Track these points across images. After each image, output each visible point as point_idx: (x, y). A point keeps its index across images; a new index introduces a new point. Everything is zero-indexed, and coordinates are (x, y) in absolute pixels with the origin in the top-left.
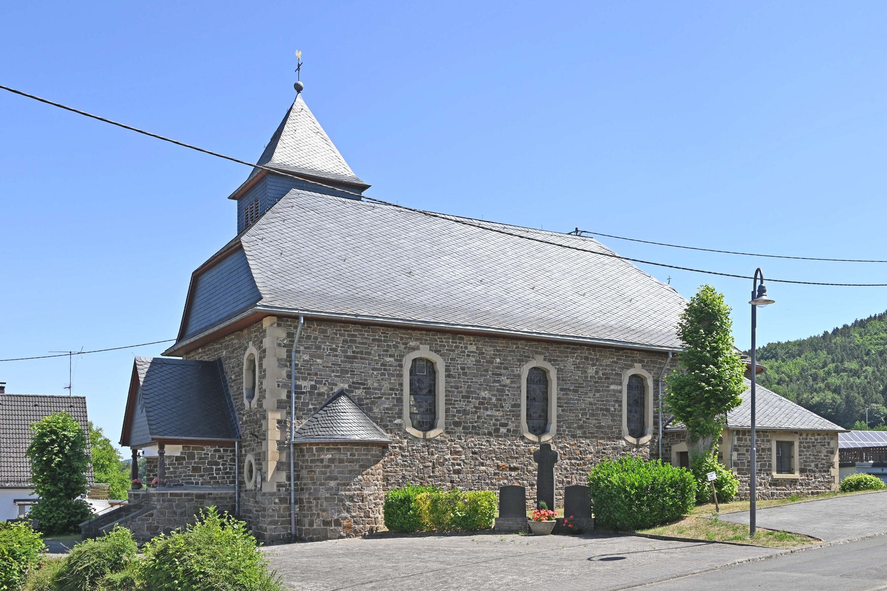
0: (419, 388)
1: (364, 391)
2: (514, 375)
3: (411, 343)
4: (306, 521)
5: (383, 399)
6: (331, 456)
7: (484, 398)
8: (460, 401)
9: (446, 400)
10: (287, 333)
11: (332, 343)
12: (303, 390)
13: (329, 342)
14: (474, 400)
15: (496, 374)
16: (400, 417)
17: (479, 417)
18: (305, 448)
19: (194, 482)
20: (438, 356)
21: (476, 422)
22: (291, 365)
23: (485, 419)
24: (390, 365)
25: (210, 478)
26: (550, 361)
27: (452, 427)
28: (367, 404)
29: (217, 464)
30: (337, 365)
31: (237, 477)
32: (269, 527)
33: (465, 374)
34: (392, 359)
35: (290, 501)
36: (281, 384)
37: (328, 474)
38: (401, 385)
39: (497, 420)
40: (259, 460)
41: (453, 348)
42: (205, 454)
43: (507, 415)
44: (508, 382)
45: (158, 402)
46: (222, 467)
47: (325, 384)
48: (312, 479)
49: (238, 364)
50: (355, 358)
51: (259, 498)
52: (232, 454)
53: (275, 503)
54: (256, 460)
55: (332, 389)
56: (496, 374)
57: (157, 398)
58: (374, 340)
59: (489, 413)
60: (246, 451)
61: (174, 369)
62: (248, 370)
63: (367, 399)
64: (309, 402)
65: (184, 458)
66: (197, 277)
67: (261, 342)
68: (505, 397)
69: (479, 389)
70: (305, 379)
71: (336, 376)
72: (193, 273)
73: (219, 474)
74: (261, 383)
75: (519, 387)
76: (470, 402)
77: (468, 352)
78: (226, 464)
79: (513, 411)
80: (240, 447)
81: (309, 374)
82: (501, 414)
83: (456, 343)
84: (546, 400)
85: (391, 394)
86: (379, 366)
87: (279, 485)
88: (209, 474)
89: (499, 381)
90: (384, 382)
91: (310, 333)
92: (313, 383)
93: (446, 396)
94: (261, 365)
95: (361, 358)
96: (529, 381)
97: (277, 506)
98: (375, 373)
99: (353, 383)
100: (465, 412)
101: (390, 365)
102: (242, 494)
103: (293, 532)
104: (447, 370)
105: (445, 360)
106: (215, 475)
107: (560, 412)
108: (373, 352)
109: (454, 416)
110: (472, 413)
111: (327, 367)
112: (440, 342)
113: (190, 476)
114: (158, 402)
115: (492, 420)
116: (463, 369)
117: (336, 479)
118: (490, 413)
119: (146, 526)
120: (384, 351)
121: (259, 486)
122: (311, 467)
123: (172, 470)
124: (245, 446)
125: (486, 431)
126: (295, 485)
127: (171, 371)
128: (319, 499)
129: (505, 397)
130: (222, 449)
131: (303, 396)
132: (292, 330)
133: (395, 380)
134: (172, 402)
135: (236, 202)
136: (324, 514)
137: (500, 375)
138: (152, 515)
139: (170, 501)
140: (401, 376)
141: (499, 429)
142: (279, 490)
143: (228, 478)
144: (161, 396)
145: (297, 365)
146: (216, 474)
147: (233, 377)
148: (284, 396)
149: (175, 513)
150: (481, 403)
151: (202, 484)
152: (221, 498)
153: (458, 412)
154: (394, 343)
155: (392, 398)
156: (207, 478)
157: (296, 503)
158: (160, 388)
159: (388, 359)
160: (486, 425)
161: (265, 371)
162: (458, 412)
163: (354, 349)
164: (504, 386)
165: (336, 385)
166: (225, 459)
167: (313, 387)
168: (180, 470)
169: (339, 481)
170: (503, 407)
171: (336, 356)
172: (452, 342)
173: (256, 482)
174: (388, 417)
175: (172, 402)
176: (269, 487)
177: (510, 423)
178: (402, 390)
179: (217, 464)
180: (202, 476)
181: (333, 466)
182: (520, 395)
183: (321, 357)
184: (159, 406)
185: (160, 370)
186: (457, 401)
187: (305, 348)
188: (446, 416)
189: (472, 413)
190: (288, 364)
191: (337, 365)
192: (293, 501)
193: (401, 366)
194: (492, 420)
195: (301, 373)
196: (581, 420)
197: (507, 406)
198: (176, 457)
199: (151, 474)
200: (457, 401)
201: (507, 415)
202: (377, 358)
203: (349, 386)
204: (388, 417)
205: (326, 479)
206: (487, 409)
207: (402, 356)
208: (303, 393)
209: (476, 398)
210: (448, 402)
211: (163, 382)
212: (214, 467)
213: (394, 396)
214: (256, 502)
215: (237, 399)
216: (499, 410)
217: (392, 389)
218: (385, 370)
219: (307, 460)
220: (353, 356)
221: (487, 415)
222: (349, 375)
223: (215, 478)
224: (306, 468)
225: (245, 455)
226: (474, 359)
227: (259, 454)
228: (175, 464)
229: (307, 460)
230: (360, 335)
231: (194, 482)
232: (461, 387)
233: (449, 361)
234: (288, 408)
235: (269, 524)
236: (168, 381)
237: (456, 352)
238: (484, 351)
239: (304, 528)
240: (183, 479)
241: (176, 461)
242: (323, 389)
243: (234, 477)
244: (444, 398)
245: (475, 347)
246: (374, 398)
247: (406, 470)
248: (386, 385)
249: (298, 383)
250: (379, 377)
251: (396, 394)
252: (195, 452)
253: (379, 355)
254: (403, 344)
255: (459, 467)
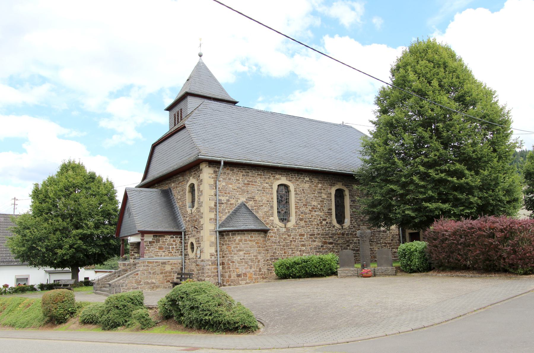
0: (281, 200)
1: (254, 202)
2: (328, 193)
3: (277, 176)
4: (227, 275)
5: (264, 206)
6: (240, 238)
7: (314, 206)
8: (302, 207)
9: (295, 207)
10: (214, 171)
11: (237, 176)
12: (222, 202)
13: (235, 176)
14: (309, 207)
15: (319, 193)
16: (272, 216)
17: (312, 216)
18: (225, 233)
19: (160, 255)
20: (291, 183)
21: (310, 218)
22: (216, 188)
23: (315, 216)
24: (267, 188)
25: (168, 252)
26: (345, 185)
27: (299, 221)
28: (256, 209)
29: (172, 245)
30: (240, 188)
31: (183, 252)
32: (206, 279)
33: (304, 193)
34: (267, 185)
35: (217, 264)
36: (211, 199)
37: (239, 248)
38: (272, 198)
39: (321, 217)
40: (198, 241)
41: (298, 179)
42: (165, 239)
43: (326, 214)
44: (325, 196)
45: (140, 211)
46: (175, 246)
47: (234, 198)
48: (229, 251)
49: (183, 190)
50: (249, 184)
51: (199, 262)
52: (180, 239)
53: (209, 265)
54: (196, 241)
55: (237, 201)
56: (319, 193)
57: (139, 209)
58: (258, 175)
59: (317, 213)
60: (189, 237)
61: (147, 194)
62: (189, 192)
63: (256, 206)
64: (225, 209)
65: (154, 242)
66: (154, 147)
67: (199, 176)
68: (324, 205)
69: (312, 201)
70: (223, 196)
71: (239, 194)
72: (152, 145)
73: (173, 250)
74: (199, 199)
75: (331, 200)
76: (307, 208)
77: (305, 181)
78: (176, 245)
79: (329, 212)
80: (185, 235)
81: (225, 193)
82: (323, 214)
83: (299, 176)
84: (343, 207)
85: (268, 204)
86: (261, 189)
87: (212, 255)
88: (168, 251)
89: (321, 197)
90: (264, 197)
91: (225, 171)
92: (227, 198)
93: (295, 204)
94: (199, 189)
95: (252, 185)
96: (336, 196)
97: (210, 267)
98: (259, 192)
99: (248, 198)
100: (306, 214)
101: (267, 188)
102: (187, 261)
103: (219, 282)
104: (295, 191)
105: (294, 185)
106: (171, 251)
107: (351, 212)
108: (258, 181)
109: (300, 215)
110: (309, 213)
111: (235, 189)
112: (291, 176)
113: (158, 252)
114: (140, 211)
115: (318, 217)
116: (303, 190)
117: (243, 251)
118: (317, 214)
119: (134, 280)
120: (263, 180)
121: (199, 256)
122: (229, 244)
123: (147, 249)
124: (187, 235)
125: (316, 223)
126: (220, 254)
127: (145, 195)
128: (234, 262)
129: (324, 205)
130: (174, 236)
131: (222, 205)
132: (217, 170)
133: (269, 196)
134: (147, 211)
135: (168, 112)
136: (237, 270)
137: (322, 193)
138: (137, 274)
139: (147, 266)
140: (272, 194)
141: (322, 222)
142: (211, 258)
143: (178, 252)
144: (141, 208)
145: (219, 188)
146: (172, 250)
147: (179, 197)
148: (213, 205)
149: (150, 273)
150: (313, 208)
151: (164, 256)
152: (175, 264)
153: (302, 213)
154: (268, 176)
155: (268, 206)
156: (167, 253)
157: (220, 264)
158: (140, 204)
159: (266, 185)
160: (315, 220)
161: (201, 192)
162: (302, 213)
163: (248, 180)
164: (324, 199)
165: (239, 199)
166: (176, 242)
167: (228, 200)
168: (152, 248)
169: (245, 252)
170: (323, 210)
171: (239, 183)
172: (297, 176)
173: (196, 254)
174: (266, 216)
175: (147, 211)
176: (206, 256)
177: (327, 219)
178: (273, 201)
179: (172, 245)
180: (164, 252)
181: (241, 243)
182: (331, 204)
183: (232, 184)
184: (140, 213)
185: (139, 194)
186: (301, 207)
187: (223, 179)
188: (296, 215)
189: (309, 213)
190: (215, 188)
191: (240, 188)
192: (219, 264)
193: (272, 188)
194: (318, 217)
195: (221, 193)
196: (361, 217)
197: (326, 210)
198: (150, 241)
199: (133, 252)
200: (301, 207)
201: (326, 214)
202: (260, 184)
203: (246, 200)
204: (266, 216)
205: (237, 251)
206: (316, 211)
207: (272, 183)
208: (222, 203)
209: (310, 206)
210: (296, 208)
211: (141, 200)
212: (171, 247)
213: (269, 204)
214: (197, 265)
215: (182, 209)
216: (321, 212)
217: (268, 201)
218: (264, 191)
219: (226, 240)
220: (248, 183)
221: (316, 215)
222: (246, 194)
223: (171, 252)
224: (226, 244)
225: (188, 239)
226: (308, 185)
227: (199, 238)
228: (149, 245)
229: (226, 240)
230: (251, 172)
231: (160, 255)
232: (302, 200)
233: (296, 186)
234: (215, 212)
235: (206, 277)
236: (144, 200)
237: (299, 181)
238: (313, 180)
239: (225, 279)
240: (153, 254)
241: (149, 243)
242: (233, 201)
243: (182, 252)
244: (295, 206)
245: (308, 178)
246: (259, 206)
247: (277, 245)
248: (265, 199)
249: (220, 198)
250: (261, 195)
251: (270, 204)
252: (160, 238)
253: (261, 183)
254: (273, 177)
255: (303, 243)
